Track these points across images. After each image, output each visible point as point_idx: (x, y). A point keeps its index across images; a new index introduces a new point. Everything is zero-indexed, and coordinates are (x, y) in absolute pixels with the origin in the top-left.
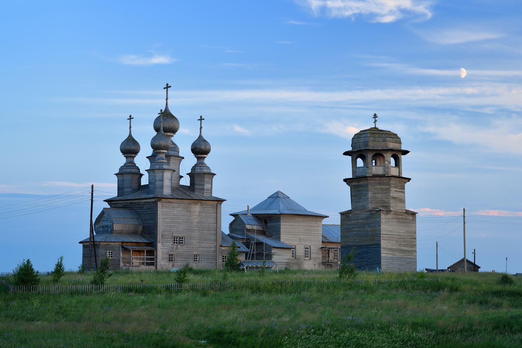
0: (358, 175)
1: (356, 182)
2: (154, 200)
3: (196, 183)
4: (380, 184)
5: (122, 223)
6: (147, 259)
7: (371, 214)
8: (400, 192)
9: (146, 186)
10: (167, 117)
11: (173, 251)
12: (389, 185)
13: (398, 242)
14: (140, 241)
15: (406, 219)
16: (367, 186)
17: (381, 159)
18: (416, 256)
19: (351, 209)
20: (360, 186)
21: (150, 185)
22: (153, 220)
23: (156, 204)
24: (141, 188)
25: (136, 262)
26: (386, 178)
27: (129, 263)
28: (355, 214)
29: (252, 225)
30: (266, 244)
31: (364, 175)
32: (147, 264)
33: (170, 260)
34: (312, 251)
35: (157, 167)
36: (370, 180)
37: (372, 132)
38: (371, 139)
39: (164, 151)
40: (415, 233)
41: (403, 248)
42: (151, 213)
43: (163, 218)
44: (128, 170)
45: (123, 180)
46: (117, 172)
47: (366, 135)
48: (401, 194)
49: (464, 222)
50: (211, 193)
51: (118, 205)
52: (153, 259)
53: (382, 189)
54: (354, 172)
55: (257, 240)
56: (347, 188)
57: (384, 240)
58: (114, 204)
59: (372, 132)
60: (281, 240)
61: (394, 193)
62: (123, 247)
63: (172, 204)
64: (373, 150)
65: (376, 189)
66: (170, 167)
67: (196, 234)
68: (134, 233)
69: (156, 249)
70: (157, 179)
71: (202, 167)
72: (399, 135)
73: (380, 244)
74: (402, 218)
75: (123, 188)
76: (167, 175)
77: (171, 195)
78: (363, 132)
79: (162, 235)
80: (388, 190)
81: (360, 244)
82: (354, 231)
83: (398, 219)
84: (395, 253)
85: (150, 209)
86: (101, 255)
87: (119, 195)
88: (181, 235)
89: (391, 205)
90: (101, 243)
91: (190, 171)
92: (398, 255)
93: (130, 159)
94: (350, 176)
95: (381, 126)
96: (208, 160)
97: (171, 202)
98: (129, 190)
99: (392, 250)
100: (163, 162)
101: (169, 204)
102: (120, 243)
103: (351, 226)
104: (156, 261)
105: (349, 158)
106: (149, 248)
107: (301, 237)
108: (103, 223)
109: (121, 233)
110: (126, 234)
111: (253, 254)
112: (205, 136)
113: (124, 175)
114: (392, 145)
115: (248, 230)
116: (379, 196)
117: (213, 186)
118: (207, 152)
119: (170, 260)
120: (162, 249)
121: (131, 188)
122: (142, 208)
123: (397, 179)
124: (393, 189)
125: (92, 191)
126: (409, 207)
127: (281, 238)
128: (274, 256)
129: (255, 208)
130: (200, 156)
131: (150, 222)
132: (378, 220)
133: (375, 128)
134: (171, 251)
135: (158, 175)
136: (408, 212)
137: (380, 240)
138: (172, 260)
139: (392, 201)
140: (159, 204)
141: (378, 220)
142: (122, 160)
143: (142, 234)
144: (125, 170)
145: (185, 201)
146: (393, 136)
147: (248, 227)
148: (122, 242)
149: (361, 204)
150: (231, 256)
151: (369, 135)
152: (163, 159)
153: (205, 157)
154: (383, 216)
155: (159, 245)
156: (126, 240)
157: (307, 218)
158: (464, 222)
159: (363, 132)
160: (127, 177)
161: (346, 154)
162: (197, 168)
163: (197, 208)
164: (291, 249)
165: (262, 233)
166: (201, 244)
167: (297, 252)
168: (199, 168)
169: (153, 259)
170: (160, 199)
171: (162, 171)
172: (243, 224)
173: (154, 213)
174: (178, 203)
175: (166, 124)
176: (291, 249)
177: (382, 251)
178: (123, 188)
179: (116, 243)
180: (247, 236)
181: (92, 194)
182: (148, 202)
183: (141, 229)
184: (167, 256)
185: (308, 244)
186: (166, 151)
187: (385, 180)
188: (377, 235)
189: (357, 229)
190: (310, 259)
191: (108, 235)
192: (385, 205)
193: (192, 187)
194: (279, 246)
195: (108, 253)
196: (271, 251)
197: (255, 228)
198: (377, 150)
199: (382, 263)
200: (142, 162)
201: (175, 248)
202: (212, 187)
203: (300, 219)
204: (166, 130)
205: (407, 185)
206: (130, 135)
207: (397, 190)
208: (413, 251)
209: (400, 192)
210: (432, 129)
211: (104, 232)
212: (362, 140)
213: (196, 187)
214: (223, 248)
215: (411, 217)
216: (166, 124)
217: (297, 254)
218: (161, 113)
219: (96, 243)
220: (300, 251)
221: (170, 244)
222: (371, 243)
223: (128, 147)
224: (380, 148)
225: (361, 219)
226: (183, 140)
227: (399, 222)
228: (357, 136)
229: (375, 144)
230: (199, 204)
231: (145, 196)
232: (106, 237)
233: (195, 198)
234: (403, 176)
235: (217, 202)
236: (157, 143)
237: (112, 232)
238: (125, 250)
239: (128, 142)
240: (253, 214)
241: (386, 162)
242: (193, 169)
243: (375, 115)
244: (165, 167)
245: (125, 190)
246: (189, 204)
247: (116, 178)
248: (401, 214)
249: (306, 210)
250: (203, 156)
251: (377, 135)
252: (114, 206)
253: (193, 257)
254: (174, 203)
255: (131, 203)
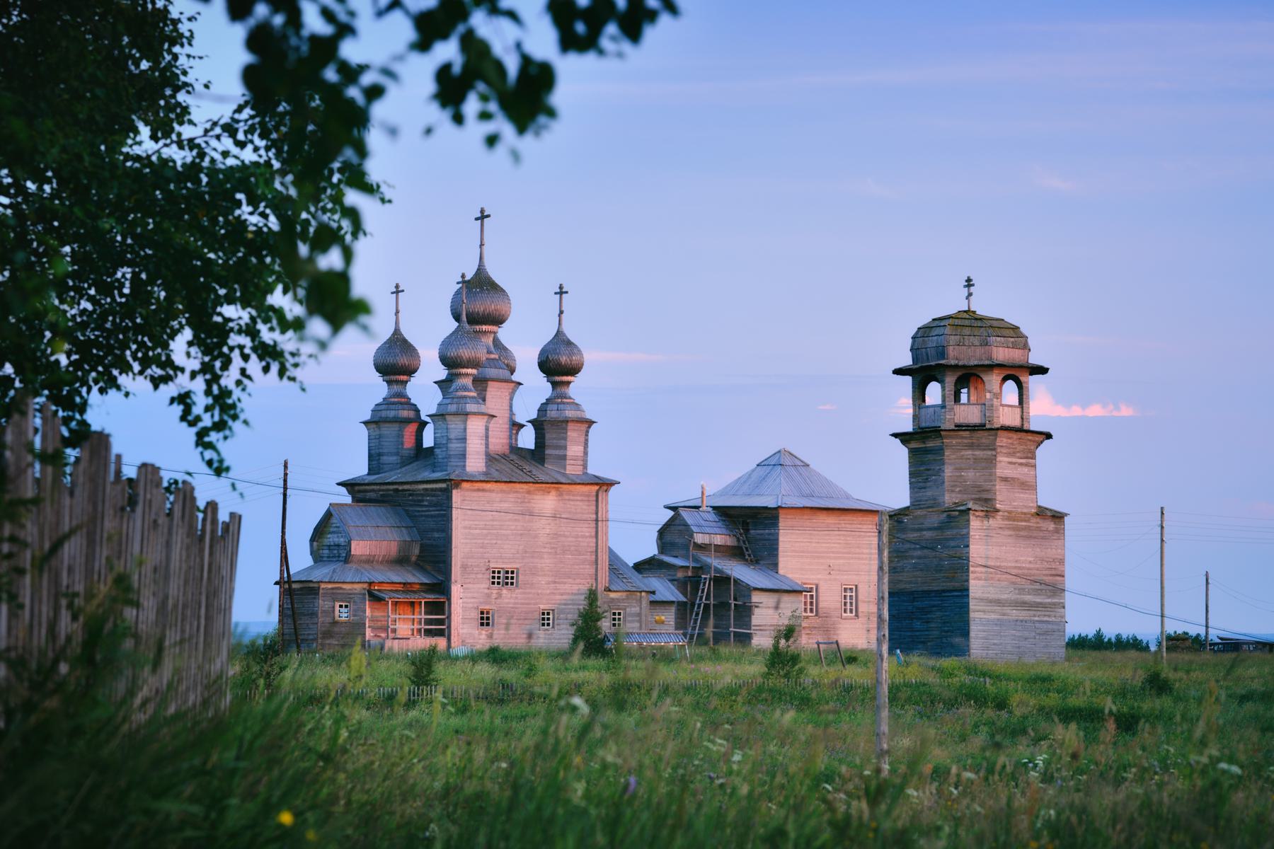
0: (923, 425)
1: (923, 442)
2: (443, 485)
3: (548, 442)
4: (971, 446)
5: (373, 540)
6: (428, 622)
7: (949, 516)
8: (1021, 464)
9: (431, 450)
10: (482, 288)
11: (490, 603)
13: (1014, 583)
14: (411, 579)
15: (1039, 529)
16: (940, 451)
18: (1063, 617)
19: (908, 504)
20: (927, 451)
21: (437, 451)
22: (443, 531)
23: (447, 493)
24: (421, 454)
25: (403, 628)
26: (986, 433)
27: (385, 629)
28: (915, 517)
29: (712, 534)
30: (737, 581)
31: (936, 424)
32: (429, 633)
33: (482, 624)
34: (860, 597)
35: (452, 408)
36: (947, 437)
37: (957, 322)
38: (953, 340)
39: (470, 371)
40: (1062, 562)
41: (1028, 598)
42: (439, 516)
43: (465, 528)
44: (392, 414)
45: (380, 436)
46: (368, 417)
48: (1026, 470)
49: (1162, 540)
50: (585, 466)
51: (369, 495)
52: (441, 622)
53: (976, 459)
54: (916, 417)
55: (717, 570)
56: (901, 454)
57: (979, 579)
58: (359, 491)
59: (957, 322)
60: (781, 572)
61: (1005, 466)
62: (371, 594)
63: (487, 494)
64: (956, 367)
65: (962, 457)
66: (483, 408)
67: (547, 562)
68: (401, 561)
69: (449, 599)
70: (452, 436)
71: (561, 406)
73: (967, 590)
74: (1026, 528)
75: (380, 455)
76: (475, 427)
77: (486, 474)
78: (937, 323)
79: (464, 567)
80: (991, 462)
81: (926, 589)
82: (913, 558)
83: (1016, 529)
84: (1007, 610)
85: (435, 505)
86: (324, 612)
87: (371, 471)
88: (509, 566)
89: (998, 498)
90: (323, 586)
91: (534, 416)
92: (1015, 614)
93: (396, 388)
94: (909, 427)
95: (983, 308)
96: (578, 387)
97: (483, 490)
98: (393, 459)
99: (998, 602)
100: (465, 397)
101: (481, 494)
102: (366, 586)
103: (908, 546)
104: (449, 627)
105: (908, 380)
106: (431, 597)
107: (831, 562)
108: (331, 539)
109: (369, 561)
110: (382, 562)
111: (707, 607)
112: (571, 333)
113: (382, 425)
114: (1001, 354)
115: (702, 547)
116: (970, 475)
117: (590, 449)
118: (574, 370)
119: (482, 624)
120: (465, 597)
121: (397, 454)
122: (418, 503)
123: (1015, 436)
124: (1002, 459)
125: (286, 475)
126: (1048, 498)
127: (781, 565)
128: (756, 611)
129: (724, 493)
130: (558, 379)
131: (436, 535)
132: (964, 531)
134: (486, 603)
135: (454, 425)
136: (1042, 513)
137: (968, 581)
138: (488, 624)
139: (1000, 487)
140: (456, 496)
141: (964, 531)
142: (379, 389)
143: (419, 565)
144: (384, 414)
145: (518, 486)
146: (1006, 332)
147: (699, 539)
148: (370, 584)
149: (929, 493)
150: (585, 621)
151: (948, 330)
152: (465, 389)
153: (569, 383)
154: (975, 523)
155: (456, 590)
156: (378, 576)
157: (849, 518)
158: (1162, 540)
159: (937, 323)
160: (389, 431)
161: (898, 372)
162: (550, 407)
163: (547, 502)
164: (801, 592)
165: (736, 553)
166: (561, 586)
167: (821, 599)
168: (555, 407)
169: (441, 622)
170: (457, 484)
171: (463, 417)
172: (686, 530)
173: (444, 515)
174: (502, 491)
175: (479, 303)
176: (801, 592)
177: (973, 605)
178: (380, 455)
179: (356, 586)
180: (696, 560)
181: (285, 481)
182: (432, 490)
183: (416, 551)
184: (477, 615)
185: (850, 579)
186: (474, 371)
187: (983, 437)
188: (960, 566)
189: (919, 553)
190: (857, 615)
191: (338, 566)
192: (985, 496)
193: (538, 455)
194: (770, 586)
195: (337, 608)
196: (750, 596)
197: (719, 540)
198: (964, 367)
199: (972, 634)
200: (424, 390)
201: (494, 596)
202: (586, 453)
203: (831, 520)
204: (474, 319)
205: (1045, 451)
206: (397, 332)
207: (1014, 460)
208: (1054, 604)
209: (1021, 464)
211: (333, 558)
213: (547, 452)
214: (612, 595)
215: (1051, 526)
216: (479, 303)
217: (821, 605)
218: (464, 282)
219: (294, 586)
220: (830, 598)
221: (482, 585)
222: (949, 585)
223: (390, 360)
224: (974, 362)
225: (930, 529)
226: (523, 339)
227: (1018, 536)
228: (924, 332)
229: (959, 353)
230: (553, 493)
231: (427, 475)
232: (334, 571)
233: (543, 478)
234: (1032, 428)
235: (597, 488)
236: (452, 353)
237: (347, 559)
238: (376, 598)
239: (390, 347)
240: (714, 508)
241: (988, 396)
242: (542, 410)
243: (969, 280)
244: (471, 407)
245: (385, 459)
246: (529, 492)
247: (364, 431)
248: (1025, 517)
249: (848, 497)
250: (565, 378)
251: (967, 331)
252: (359, 495)
253: (537, 616)
254: (490, 491)
255: (397, 490)
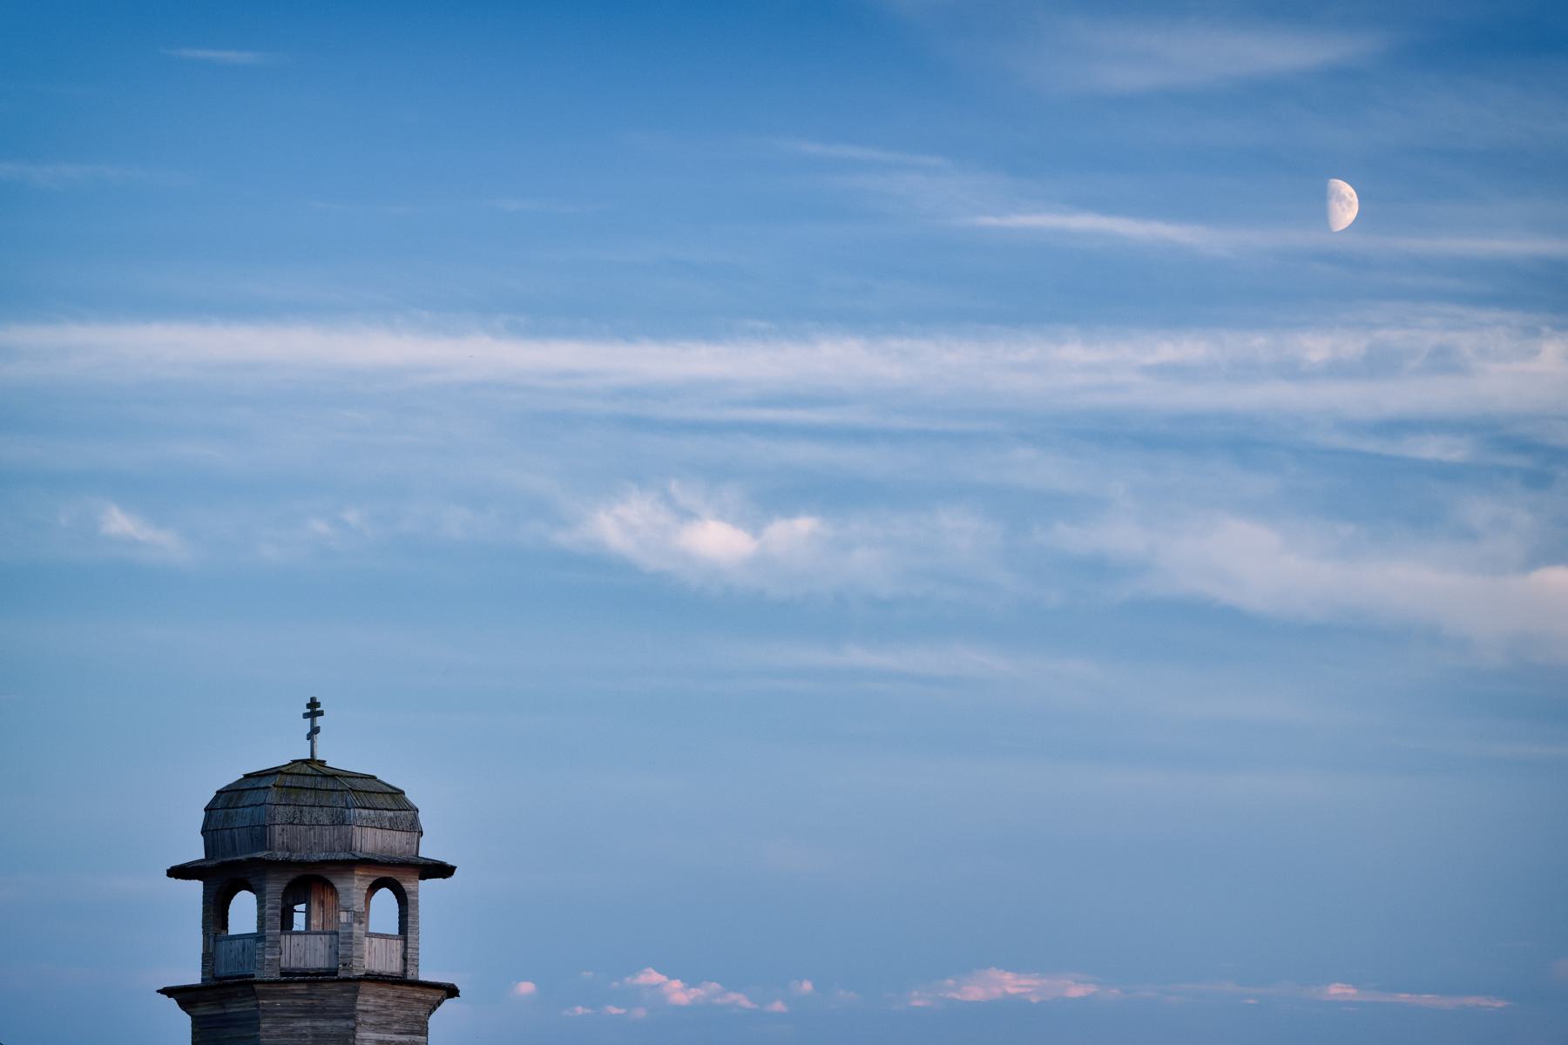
0: (222, 972)
4: (310, 1012)
12: (353, 1017)
16: (252, 1021)
17: (329, 899)
26: (337, 988)
36: (265, 995)
47: (260, 797)
54: (208, 958)
59: (289, 781)
64: (286, 864)
72: (412, 796)
95: (336, 754)
114: (371, 840)
133: (310, 762)
146: (380, 800)
151: (272, 796)
187: (334, 996)
210: (1119, 536)
212: (243, 817)
241: (344, 917)
251: (308, 798)
